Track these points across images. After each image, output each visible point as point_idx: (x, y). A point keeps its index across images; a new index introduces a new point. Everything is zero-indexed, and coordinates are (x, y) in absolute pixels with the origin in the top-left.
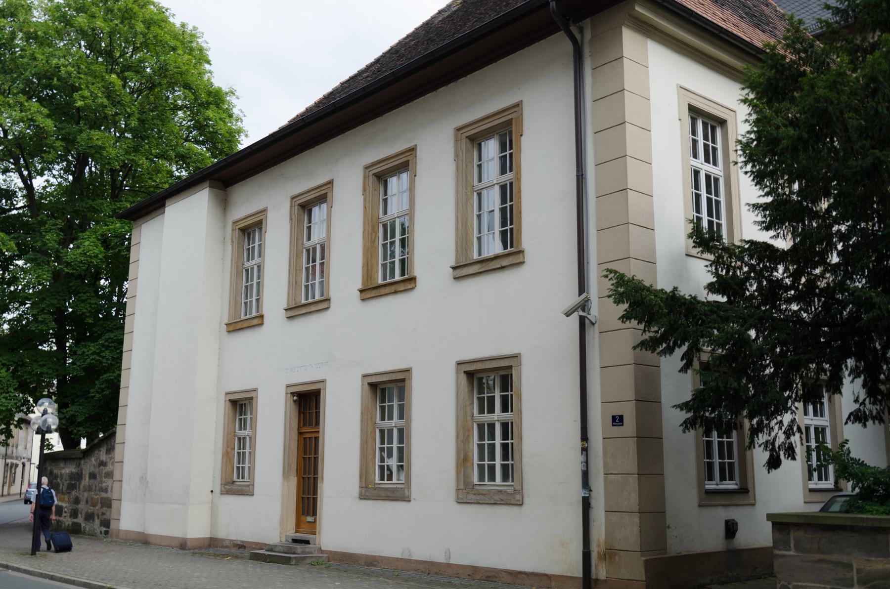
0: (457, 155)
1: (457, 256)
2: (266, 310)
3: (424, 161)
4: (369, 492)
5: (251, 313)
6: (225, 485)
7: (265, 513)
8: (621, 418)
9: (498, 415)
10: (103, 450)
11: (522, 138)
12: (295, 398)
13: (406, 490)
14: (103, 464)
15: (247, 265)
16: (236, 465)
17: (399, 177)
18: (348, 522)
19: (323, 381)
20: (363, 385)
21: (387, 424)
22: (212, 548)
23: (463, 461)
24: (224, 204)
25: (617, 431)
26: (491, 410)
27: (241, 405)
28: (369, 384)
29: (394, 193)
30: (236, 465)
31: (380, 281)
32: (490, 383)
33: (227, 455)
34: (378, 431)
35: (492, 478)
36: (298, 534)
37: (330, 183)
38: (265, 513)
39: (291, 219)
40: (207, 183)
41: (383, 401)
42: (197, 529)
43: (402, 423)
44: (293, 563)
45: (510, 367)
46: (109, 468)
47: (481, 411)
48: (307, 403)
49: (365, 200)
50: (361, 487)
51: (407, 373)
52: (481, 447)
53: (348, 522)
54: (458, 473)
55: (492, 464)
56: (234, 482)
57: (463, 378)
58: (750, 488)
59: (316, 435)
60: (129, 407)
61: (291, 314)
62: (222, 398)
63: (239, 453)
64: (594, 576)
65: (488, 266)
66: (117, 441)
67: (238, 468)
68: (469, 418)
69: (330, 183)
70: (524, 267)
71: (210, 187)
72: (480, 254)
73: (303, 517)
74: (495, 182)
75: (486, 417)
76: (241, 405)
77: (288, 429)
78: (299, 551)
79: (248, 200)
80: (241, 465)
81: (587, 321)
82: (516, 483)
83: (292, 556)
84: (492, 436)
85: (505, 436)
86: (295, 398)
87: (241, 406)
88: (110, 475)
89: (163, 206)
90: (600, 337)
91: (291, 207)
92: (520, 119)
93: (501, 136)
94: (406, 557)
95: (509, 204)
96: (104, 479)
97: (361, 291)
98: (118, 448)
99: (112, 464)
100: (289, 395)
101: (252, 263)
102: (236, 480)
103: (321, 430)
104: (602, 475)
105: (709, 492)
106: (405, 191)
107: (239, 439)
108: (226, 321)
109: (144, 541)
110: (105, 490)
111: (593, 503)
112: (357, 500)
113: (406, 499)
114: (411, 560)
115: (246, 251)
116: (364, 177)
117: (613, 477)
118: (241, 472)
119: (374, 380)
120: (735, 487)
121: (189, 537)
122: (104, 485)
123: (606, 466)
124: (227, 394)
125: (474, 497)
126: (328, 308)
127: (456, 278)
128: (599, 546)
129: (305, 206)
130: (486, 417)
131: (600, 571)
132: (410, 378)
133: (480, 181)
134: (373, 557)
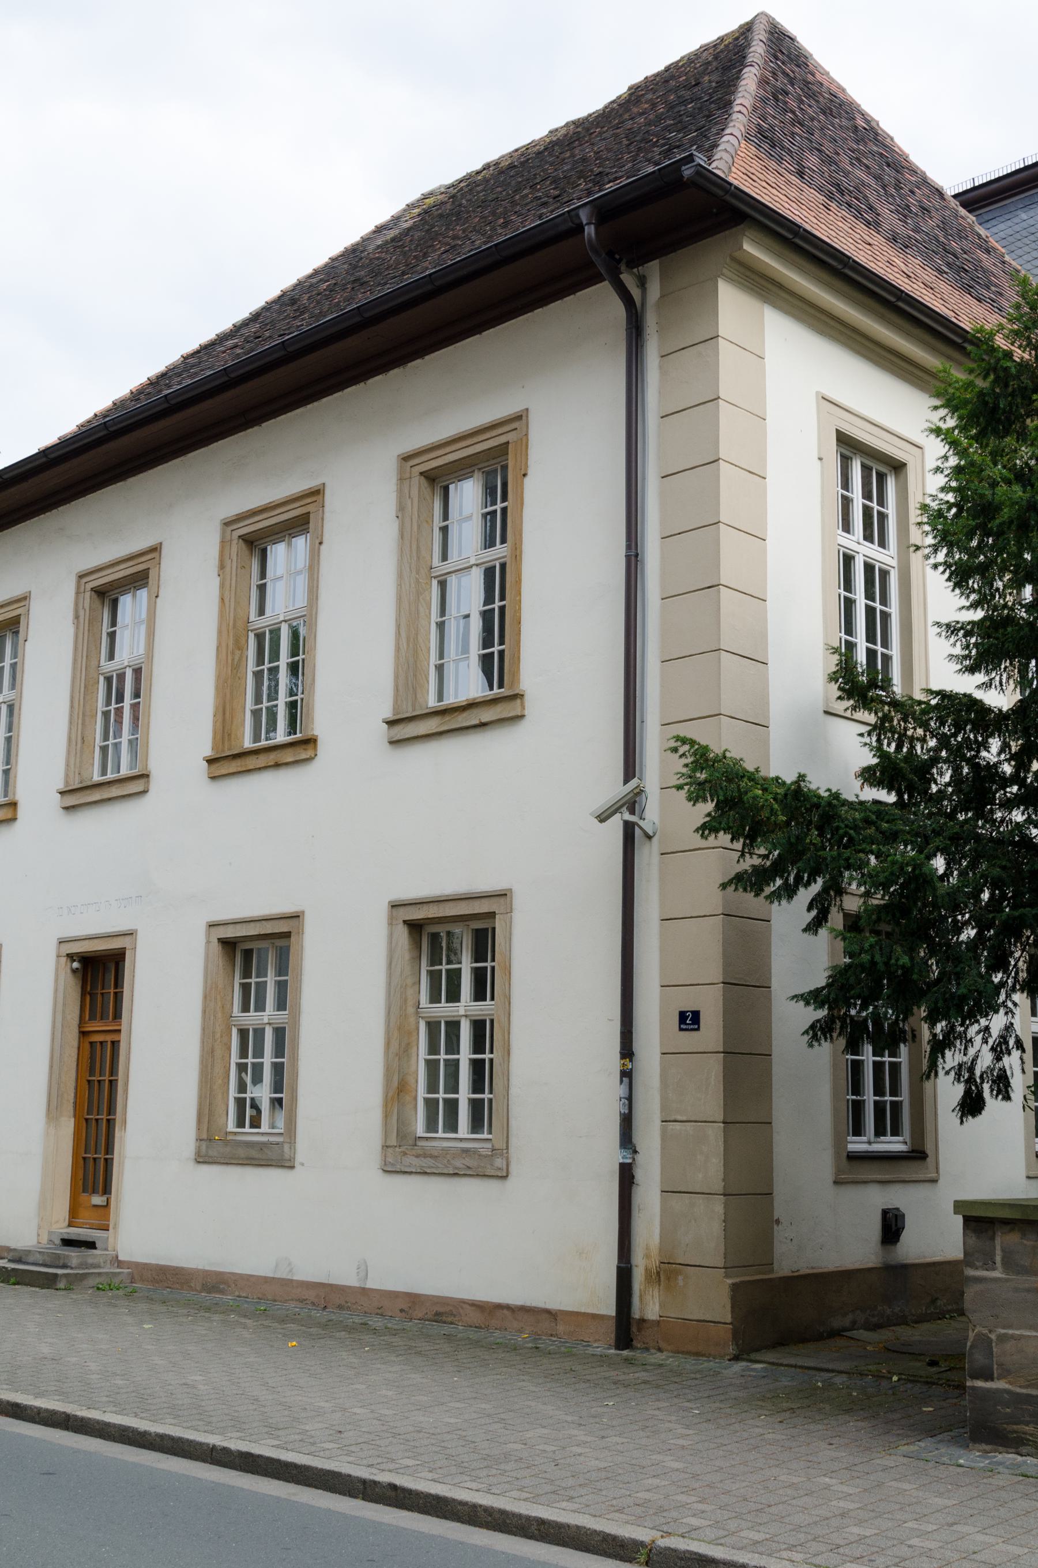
0: (401, 508)
1: (67, 776)
3: (337, 515)
4: (214, 1149)
9: (466, 1007)
11: (526, 480)
12: (76, 965)
13: (286, 1147)
18: (171, 1205)
19: (130, 934)
20: (208, 942)
21: (252, 1019)
23: (397, 1092)
25: (689, 1040)
26: (454, 996)
31: (248, 744)
32: (453, 944)
34: (235, 1032)
35: (452, 1125)
36: (73, 1230)
39: (77, 617)
43: (281, 1017)
44: (62, 1285)
45: (492, 915)
47: (435, 998)
49: (222, 586)
50: (199, 1140)
51: (128, 939)
52: (432, 1066)
53: (171, 1205)
54: (386, 1116)
55: (454, 1094)
61: (72, 800)
64: (636, 1314)
65: (455, 720)
68: (411, 1010)
72: (440, 698)
73: (84, 1197)
75: (444, 1010)
77: (59, 1025)
78: (74, 1262)
83: (60, 1271)
84: (453, 1046)
85: (478, 1045)
86: (76, 965)
91: (77, 593)
92: (524, 443)
100: (64, 960)
104: (657, 1123)
111: (639, 1174)
112: (192, 1163)
119: (230, 933)
126: (145, 792)
128: (647, 1256)
130: (444, 1010)
131: (649, 1305)
132: (300, 932)
133: (444, 557)
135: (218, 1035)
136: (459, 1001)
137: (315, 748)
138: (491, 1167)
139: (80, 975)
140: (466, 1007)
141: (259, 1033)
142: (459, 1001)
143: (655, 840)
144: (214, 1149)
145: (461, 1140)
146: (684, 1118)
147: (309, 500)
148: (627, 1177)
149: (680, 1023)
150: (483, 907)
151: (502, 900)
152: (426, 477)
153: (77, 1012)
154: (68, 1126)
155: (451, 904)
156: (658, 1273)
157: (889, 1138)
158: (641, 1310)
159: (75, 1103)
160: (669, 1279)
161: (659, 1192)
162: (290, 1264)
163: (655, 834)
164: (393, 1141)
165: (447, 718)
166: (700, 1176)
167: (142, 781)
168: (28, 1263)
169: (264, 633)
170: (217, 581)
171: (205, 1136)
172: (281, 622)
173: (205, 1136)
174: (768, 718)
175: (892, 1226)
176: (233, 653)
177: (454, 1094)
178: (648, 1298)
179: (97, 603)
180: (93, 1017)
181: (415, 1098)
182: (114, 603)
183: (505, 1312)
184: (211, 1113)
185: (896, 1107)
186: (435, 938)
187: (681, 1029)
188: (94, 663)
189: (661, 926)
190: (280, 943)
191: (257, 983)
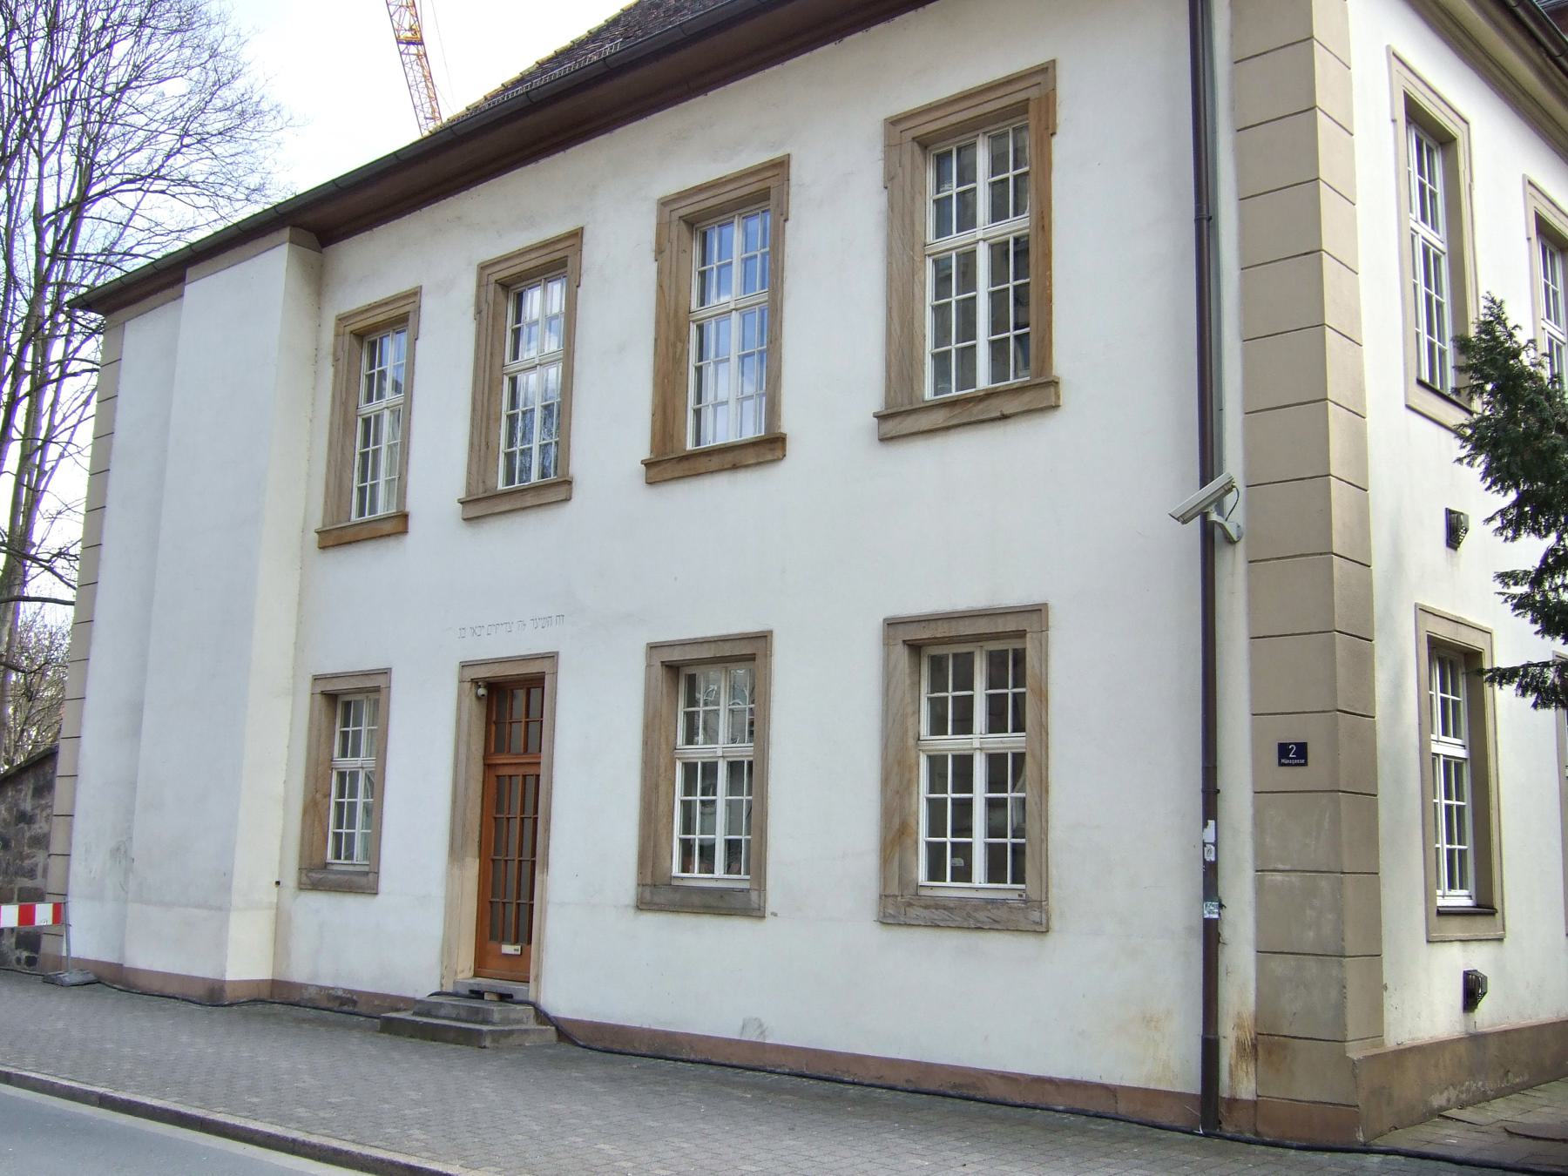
1: (469, 484)
2: (415, 504)
4: (657, 894)
5: (373, 510)
6: (311, 870)
7: (1087, 993)
8: (1302, 750)
9: (980, 741)
10: (27, 788)
11: (1055, 140)
12: (482, 691)
13: (754, 895)
14: (24, 818)
15: (367, 409)
16: (332, 829)
17: (545, 290)
18: (600, 952)
19: (552, 657)
20: (649, 666)
21: (348, 763)
22: (281, 1003)
23: (895, 837)
24: (318, 280)
25: (1292, 777)
27: (347, 705)
28: (323, 693)
29: (535, 317)
30: (332, 829)
32: (971, 668)
33: (313, 809)
34: (679, 766)
35: (963, 874)
36: (479, 980)
37: (577, 235)
38: (408, 930)
40: (286, 233)
41: (346, 724)
42: (245, 961)
44: (487, 1043)
45: (1021, 634)
46: (39, 827)
47: (938, 727)
48: (508, 705)
49: (660, 272)
50: (641, 885)
51: (547, 662)
52: (936, 808)
53: (600, 952)
55: (972, 840)
56: (326, 865)
57: (902, 656)
58: (1498, 906)
59: (531, 770)
60: (88, 701)
61: (475, 511)
62: (306, 687)
63: (340, 806)
64: (1225, 1091)
65: (966, 412)
66: (59, 773)
67: (338, 836)
68: (911, 742)
69: (577, 235)
70: (1058, 414)
71: (291, 242)
72: (698, 442)
73: (492, 945)
74: (732, 306)
75: (951, 743)
76: (347, 705)
77: (463, 757)
78: (496, 1017)
79: (376, 267)
80: (344, 831)
81: (1218, 532)
82: (1030, 886)
83: (485, 1028)
84: (710, 788)
86: (482, 691)
87: (348, 706)
88: (41, 842)
89: (181, 280)
90: (1249, 572)
93: (993, 138)
94: (752, 1036)
95: (372, 447)
96: (27, 850)
97: (882, 417)
98: (60, 785)
99: (48, 818)
100: (467, 685)
101: (375, 406)
102: (335, 858)
103: (544, 760)
104: (1249, 873)
105: (1443, 913)
106: (556, 317)
107: (342, 775)
108: (318, 525)
109: (113, 981)
110: (31, 874)
111: (1226, 932)
112: (631, 912)
113: (373, 891)
114: (763, 1045)
115: (364, 381)
116: (659, 225)
117: (1278, 877)
118: (343, 846)
119: (676, 656)
120: (1468, 902)
121: (230, 977)
122: (27, 863)
123: (1260, 851)
124: (316, 679)
125: (925, 913)
126: (568, 499)
127: (885, 439)
128: (1239, 1026)
129: (506, 286)
130: (951, 743)
131: (1240, 1082)
132: (1044, 629)
133: (702, 303)
134: (668, 1035)
135: (662, 770)
136: (971, 732)
137: (784, 449)
138: (1030, 918)
139: (484, 702)
140: (980, 741)
141: (354, 775)
142: (971, 732)
143: (1240, 547)
144: (657, 894)
145: (977, 889)
146: (1288, 867)
147: (769, 174)
148: (1211, 935)
149: (1280, 758)
150: (1011, 625)
151: (1035, 616)
152: (686, 222)
153: (482, 743)
154: (472, 868)
155: (967, 622)
156: (1254, 1046)
157: (1458, 892)
158: (1232, 1088)
159: (480, 842)
160: (1270, 1053)
161: (1253, 953)
162: (761, 1025)
163: (1239, 538)
164: (894, 889)
165: (957, 410)
166: (1311, 934)
167: (564, 488)
168: (436, 1017)
169: (1007, 242)
170: (654, 266)
171: (649, 881)
172: (977, 242)
173: (649, 881)
174: (1364, 407)
175: (1473, 990)
176: (674, 345)
177: (972, 840)
178: (1241, 1074)
179: (501, 296)
180: (499, 750)
181: (917, 843)
182: (519, 300)
183: (1048, 1086)
184: (656, 856)
185: (351, 837)
186: (938, 664)
187: (1281, 764)
188: (352, 408)
189: (1251, 645)
190: (372, 696)
191: (1015, 695)
